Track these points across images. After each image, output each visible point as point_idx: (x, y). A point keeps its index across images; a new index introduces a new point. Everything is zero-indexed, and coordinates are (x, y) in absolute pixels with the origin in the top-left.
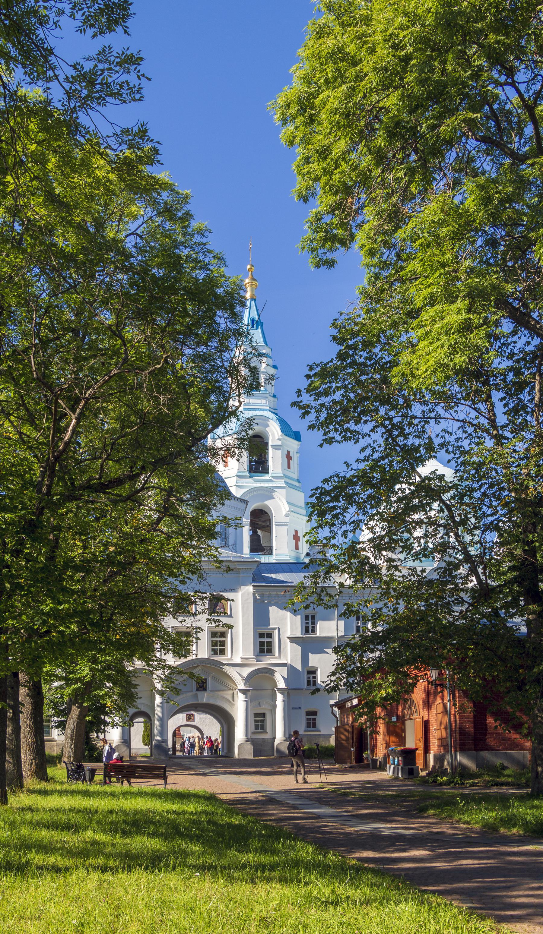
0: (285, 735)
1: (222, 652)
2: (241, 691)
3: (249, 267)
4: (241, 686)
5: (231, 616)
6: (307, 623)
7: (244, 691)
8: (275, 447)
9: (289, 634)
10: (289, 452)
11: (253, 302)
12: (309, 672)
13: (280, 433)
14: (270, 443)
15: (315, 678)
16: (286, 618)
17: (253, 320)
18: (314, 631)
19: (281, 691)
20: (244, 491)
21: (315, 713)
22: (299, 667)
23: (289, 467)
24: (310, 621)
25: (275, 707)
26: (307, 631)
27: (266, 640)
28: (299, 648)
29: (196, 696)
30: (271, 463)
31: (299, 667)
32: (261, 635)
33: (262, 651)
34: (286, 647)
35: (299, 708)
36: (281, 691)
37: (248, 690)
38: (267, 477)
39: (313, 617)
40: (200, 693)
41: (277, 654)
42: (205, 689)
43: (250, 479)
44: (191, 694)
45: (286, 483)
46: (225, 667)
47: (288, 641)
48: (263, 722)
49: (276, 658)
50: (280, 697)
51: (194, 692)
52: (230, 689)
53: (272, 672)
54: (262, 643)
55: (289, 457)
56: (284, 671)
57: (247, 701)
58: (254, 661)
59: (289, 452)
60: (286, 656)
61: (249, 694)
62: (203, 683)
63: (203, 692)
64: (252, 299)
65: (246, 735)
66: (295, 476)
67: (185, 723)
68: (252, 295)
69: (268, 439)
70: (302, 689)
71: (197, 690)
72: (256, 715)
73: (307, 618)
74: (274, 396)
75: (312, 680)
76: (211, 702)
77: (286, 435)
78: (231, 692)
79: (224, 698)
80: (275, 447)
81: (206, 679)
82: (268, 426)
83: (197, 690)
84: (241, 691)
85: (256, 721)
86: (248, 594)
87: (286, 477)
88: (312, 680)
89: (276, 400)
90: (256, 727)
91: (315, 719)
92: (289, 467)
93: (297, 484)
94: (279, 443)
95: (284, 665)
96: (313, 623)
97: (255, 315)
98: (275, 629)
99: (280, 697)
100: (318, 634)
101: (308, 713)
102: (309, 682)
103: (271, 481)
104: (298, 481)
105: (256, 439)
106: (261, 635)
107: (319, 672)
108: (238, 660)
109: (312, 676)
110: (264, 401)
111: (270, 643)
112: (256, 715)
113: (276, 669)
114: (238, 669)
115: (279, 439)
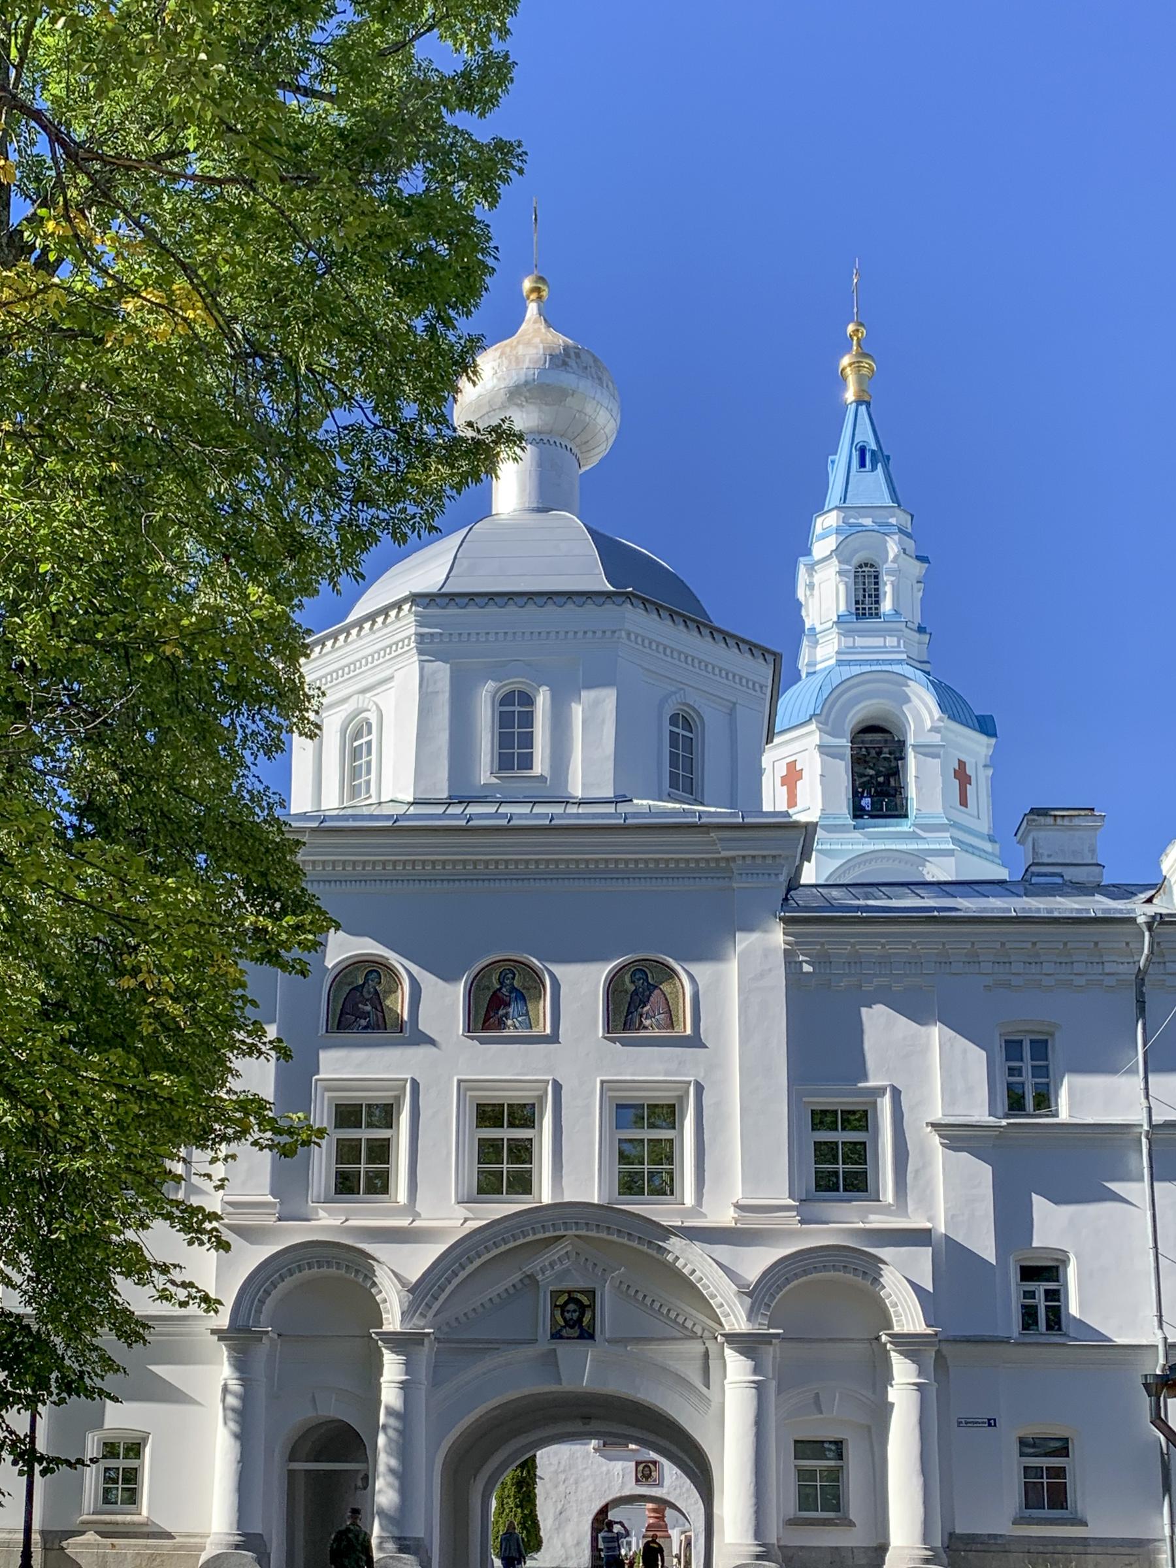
0: (926, 1536)
1: (665, 1187)
2: (734, 1340)
3: (851, 328)
4: (737, 1320)
5: (695, 1041)
6: (1012, 1071)
7: (747, 1344)
8: (926, 751)
9: (938, 1116)
10: (962, 764)
11: (863, 408)
12: (1029, 1273)
13: (937, 712)
14: (911, 740)
15: (1052, 1295)
16: (925, 1049)
17: (862, 451)
18: (1044, 1101)
19: (910, 1345)
20: (838, 863)
21: (1062, 1448)
22: (985, 1247)
23: (964, 802)
24: (1027, 1064)
25: (885, 1409)
26: (1016, 1104)
27: (841, 1137)
28: (985, 1171)
29: (550, 1359)
30: (912, 791)
31: (985, 1247)
32: (822, 1119)
33: (826, 1184)
34: (926, 1164)
35: (992, 1423)
36: (910, 1345)
37: (766, 1339)
38: (905, 826)
39: (1041, 1048)
40: (565, 1350)
41: (888, 1194)
42: (587, 1335)
43: (857, 835)
44: (530, 1351)
45: (955, 840)
46: (675, 1245)
47: (936, 1140)
48: (835, 1475)
49: (886, 1210)
50: (903, 1371)
51: (544, 1344)
52: (693, 1336)
53: (871, 1269)
54: (825, 1152)
55: (962, 775)
56: (921, 1262)
57: (759, 1387)
58: (791, 1221)
59: (962, 764)
60: (927, 1203)
61: (770, 1353)
62: (582, 1308)
63: (579, 1347)
64: (859, 402)
65: (758, 1533)
66: (984, 826)
67: (632, 1489)
68: (861, 390)
69: (905, 734)
70: (1005, 1341)
71: (556, 1335)
72: (805, 1448)
73: (1013, 1048)
74: (921, 630)
75: (1042, 1304)
76: (616, 1386)
77: (952, 717)
78: (696, 1348)
79: (665, 1370)
80: (926, 751)
81: (591, 1293)
82: (907, 700)
83: (556, 1335)
84: (734, 1340)
85: (804, 1475)
86: (767, 953)
87: (955, 825)
88: (1042, 1304)
89: (926, 638)
90: (806, 1500)
91: (1060, 1472)
92: (964, 802)
93: (988, 846)
94: (936, 739)
95: (920, 1237)
96: (1042, 1071)
97: (866, 436)
98: (880, 1091)
99: (903, 1371)
100: (1064, 1116)
101: (1027, 1445)
102: (1029, 1316)
103: (913, 836)
104: (991, 839)
105: (869, 737)
106: (822, 1119)
107: (1072, 1273)
108: (726, 1217)
109: (1041, 1287)
110: (891, 641)
111: (859, 1153)
112: (805, 1448)
113: (883, 1253)
114: (723, 1252)
115: (934, 729)
